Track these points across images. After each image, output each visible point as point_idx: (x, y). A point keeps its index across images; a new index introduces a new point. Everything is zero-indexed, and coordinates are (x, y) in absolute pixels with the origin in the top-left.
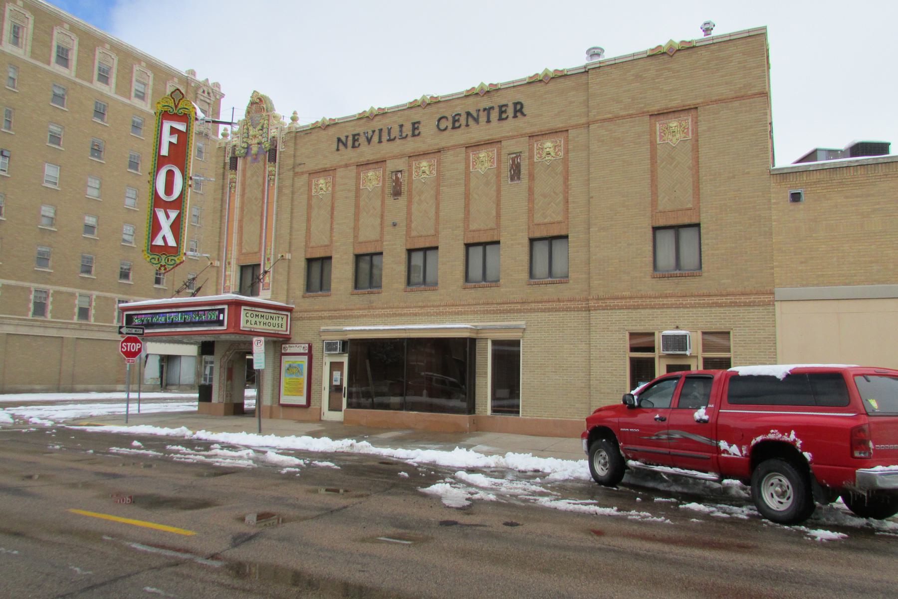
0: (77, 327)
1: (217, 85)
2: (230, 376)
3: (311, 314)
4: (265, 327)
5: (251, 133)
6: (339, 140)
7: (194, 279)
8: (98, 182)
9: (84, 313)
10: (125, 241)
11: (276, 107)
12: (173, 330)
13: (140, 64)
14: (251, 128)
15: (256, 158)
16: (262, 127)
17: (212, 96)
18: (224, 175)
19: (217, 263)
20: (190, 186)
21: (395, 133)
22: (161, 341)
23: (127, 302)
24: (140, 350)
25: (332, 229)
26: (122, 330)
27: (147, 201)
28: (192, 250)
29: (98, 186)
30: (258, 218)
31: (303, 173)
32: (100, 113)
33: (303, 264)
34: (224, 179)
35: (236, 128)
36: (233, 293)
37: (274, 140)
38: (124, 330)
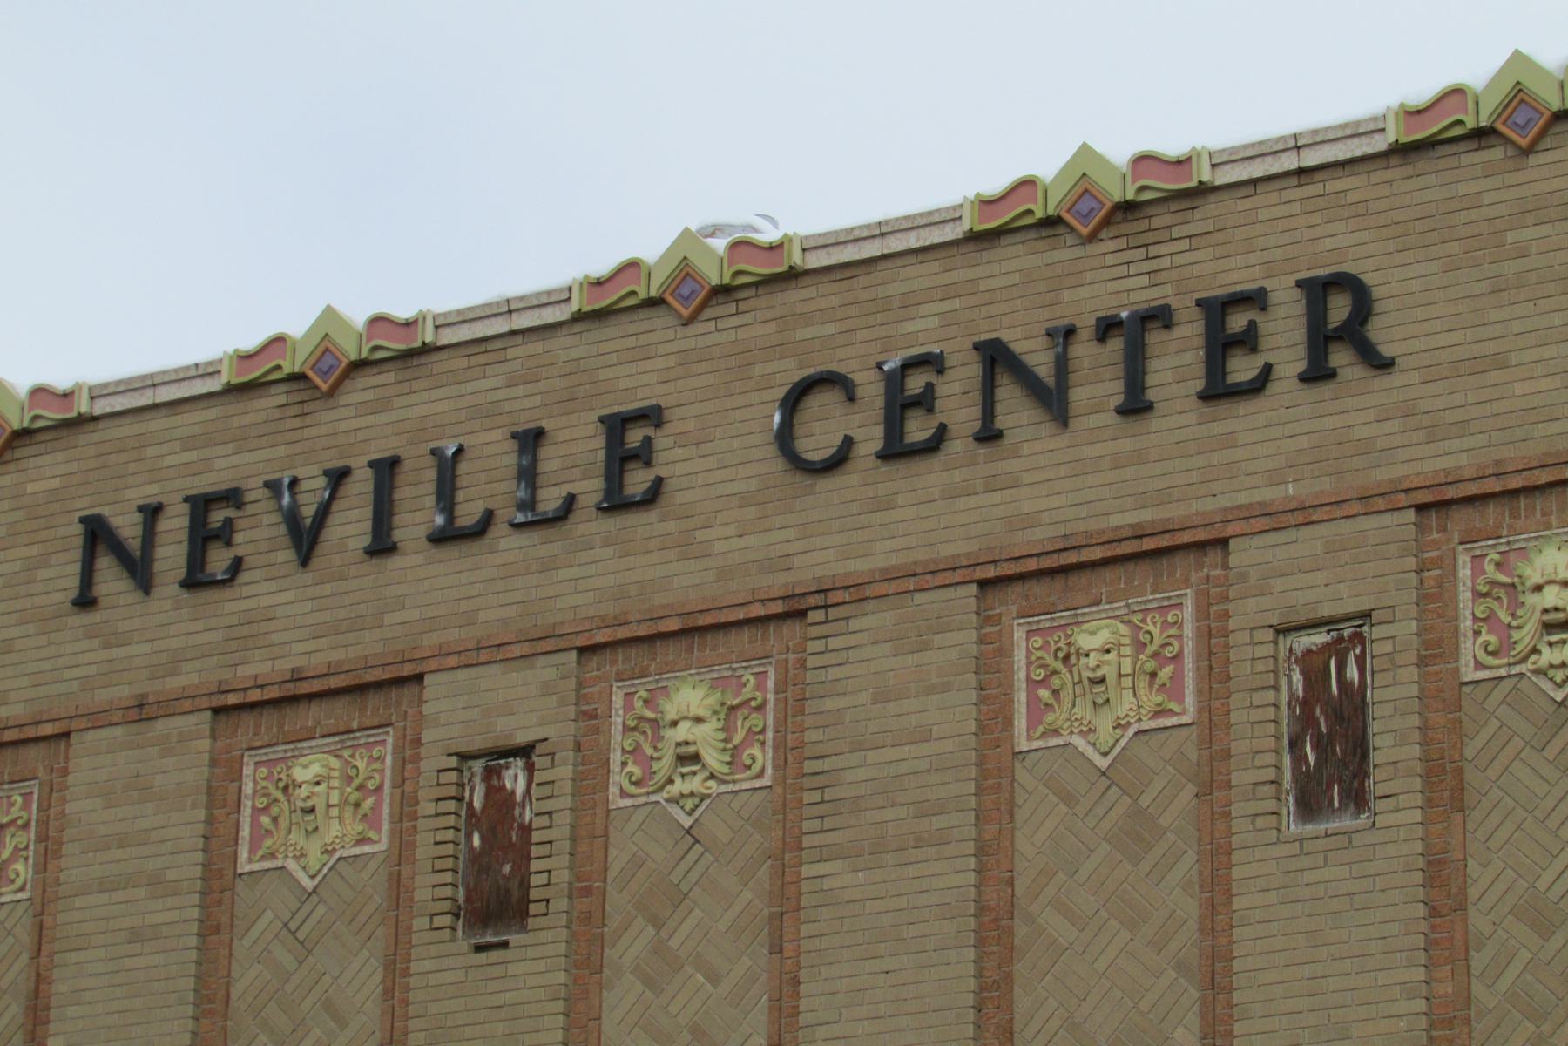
6: (97, 533)
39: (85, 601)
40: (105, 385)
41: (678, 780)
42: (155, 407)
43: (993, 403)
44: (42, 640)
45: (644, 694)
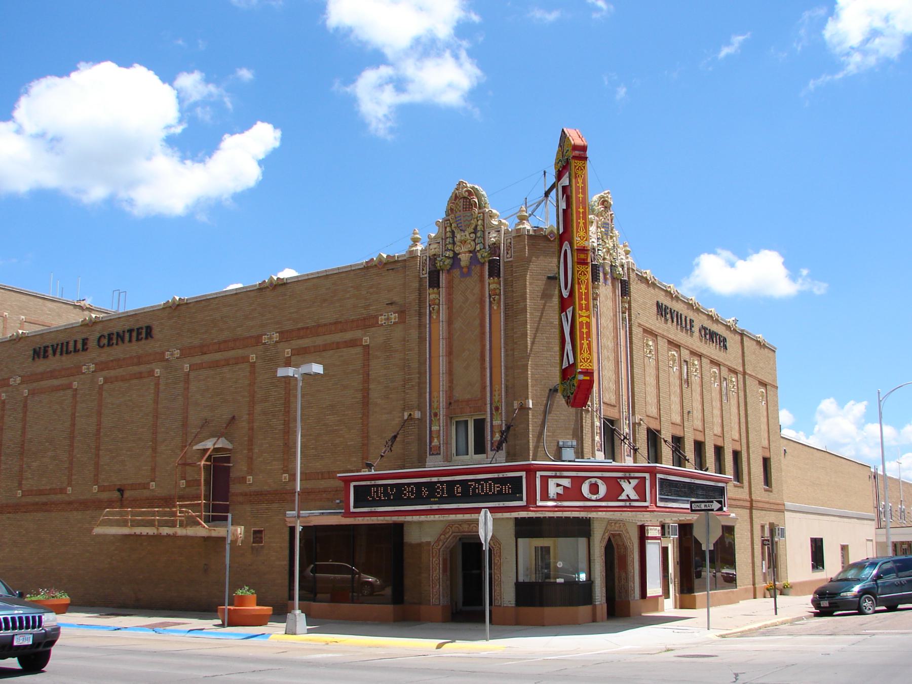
5: (458, 237)
15: (467, 273)
21: (71, 348)
37: (495, 248)
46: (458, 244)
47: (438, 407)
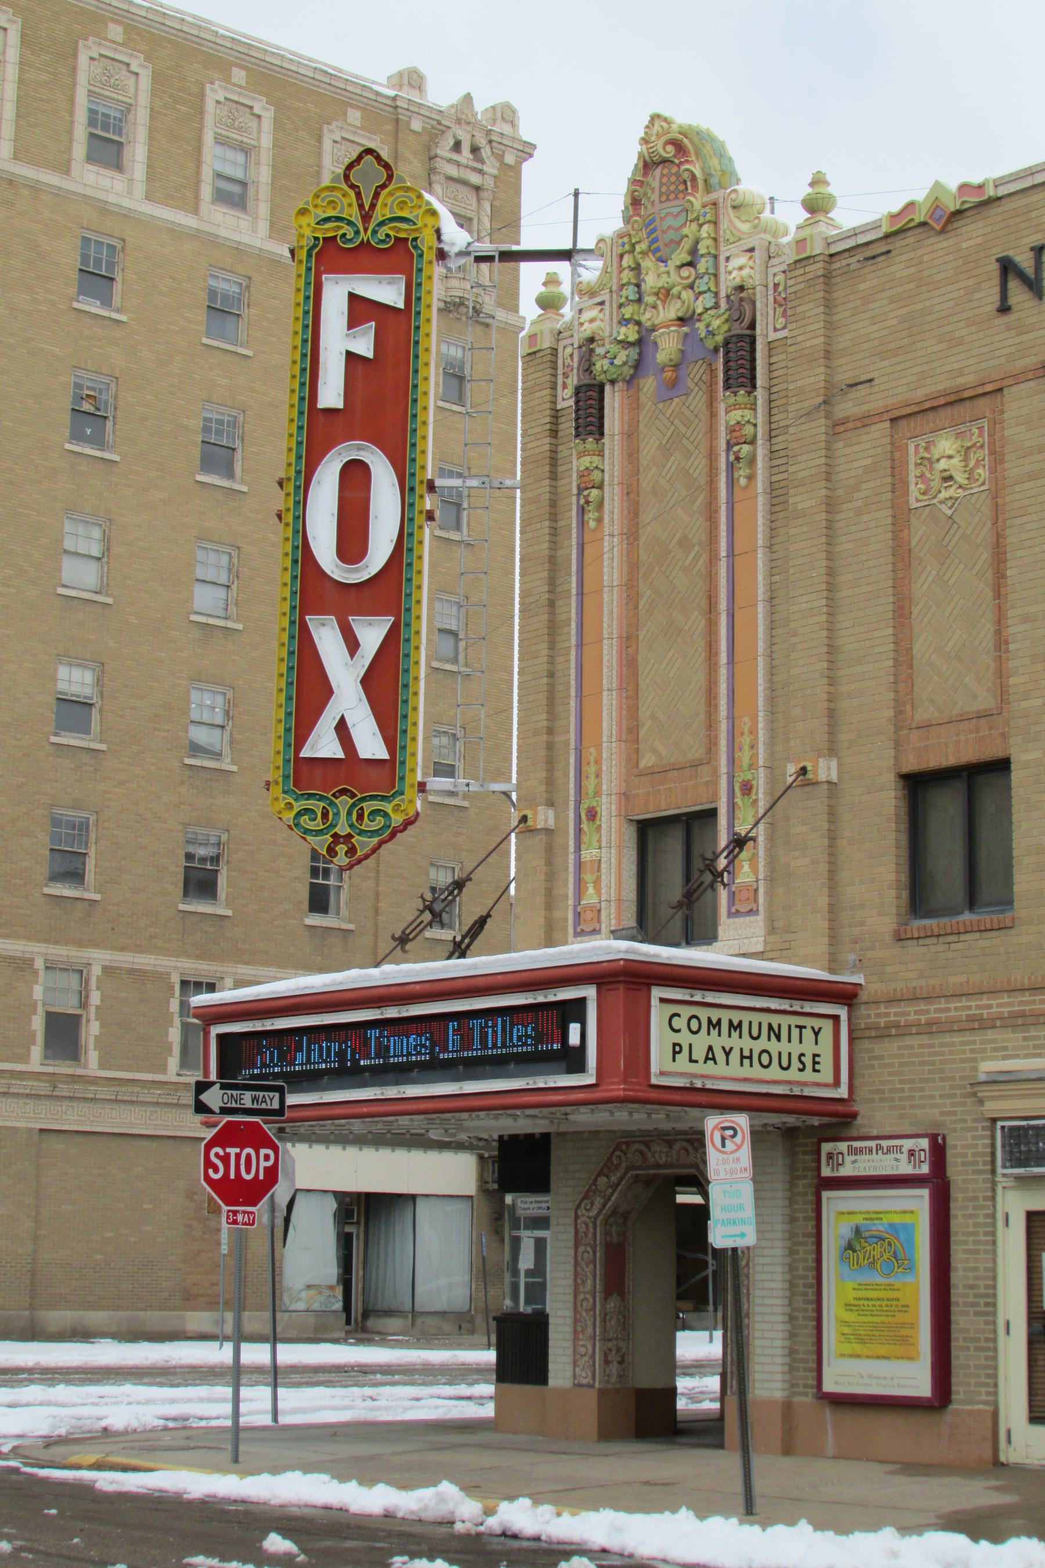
0: (43, 1087)
1: (507, 114)
2: (615, 1281)
3: (933, 1011)
4: (746, 1071)
5: (651, 281)
6: (1007, 267)
7: (459, 885)
8: (97, 533)
9: (63, 1034)
10: (196, 749)
11: (741, 168)
12: (392, 1092)
13: (228, 80)
14: (648, 263)
16: (694, 251)
17: (489, 155)
18: (554, 460)
19: (544, 817)
20: (430, 516)
22: (344, 1140)
23: (211, 988)
24: (272, 1174)
25: (1001, 643)
26: (205, 1097)
27: (276, 586)
28: (448, 771)
29: (96, 551)
30: (697, 622)
31: (865, 421)
32: (96, 279)
33: (888, 800)
34: (554, 476)
35: (591, 271)
36: (616, 934)
38: (213, 1098)
39: (1004, 309)
40: (1003, 178)
41: (943, 490)
42: (1034, 187)
43: (1001, 292)
44: (981, 335)
45: (924, 445)
46: (649, 299)
47: (753, 766)
